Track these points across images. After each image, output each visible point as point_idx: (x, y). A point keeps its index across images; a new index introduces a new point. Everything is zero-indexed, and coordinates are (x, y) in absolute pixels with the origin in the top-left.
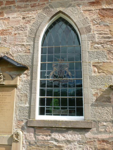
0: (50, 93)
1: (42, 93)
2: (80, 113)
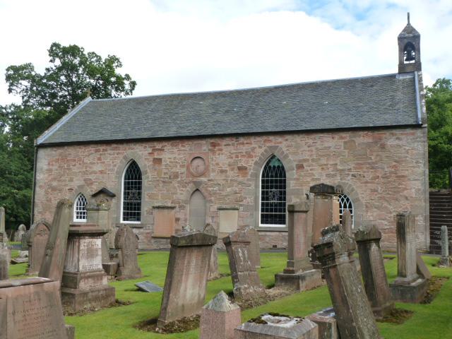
0: (267, 211)
1: (262, 210)
2: (139, 220)
